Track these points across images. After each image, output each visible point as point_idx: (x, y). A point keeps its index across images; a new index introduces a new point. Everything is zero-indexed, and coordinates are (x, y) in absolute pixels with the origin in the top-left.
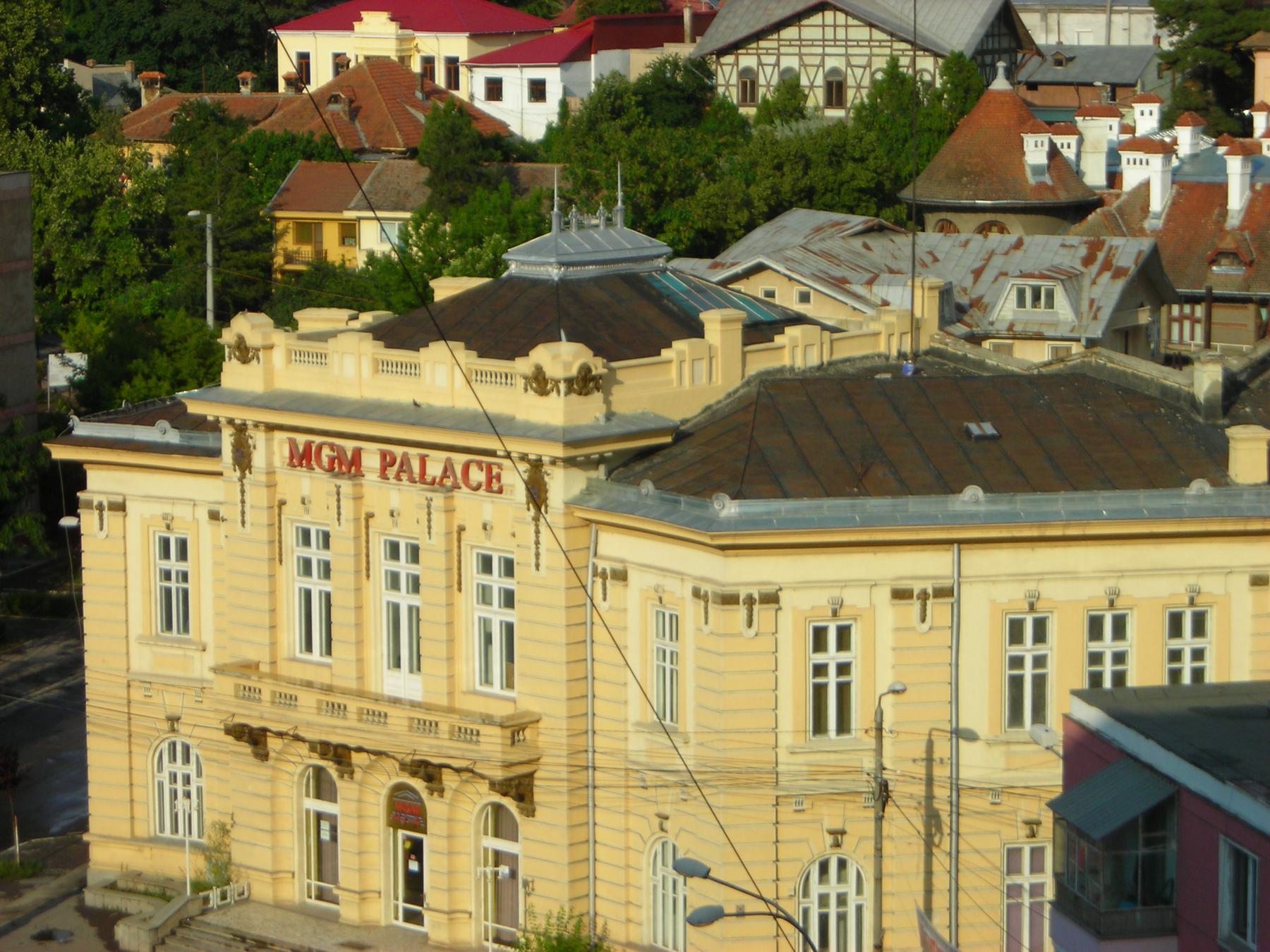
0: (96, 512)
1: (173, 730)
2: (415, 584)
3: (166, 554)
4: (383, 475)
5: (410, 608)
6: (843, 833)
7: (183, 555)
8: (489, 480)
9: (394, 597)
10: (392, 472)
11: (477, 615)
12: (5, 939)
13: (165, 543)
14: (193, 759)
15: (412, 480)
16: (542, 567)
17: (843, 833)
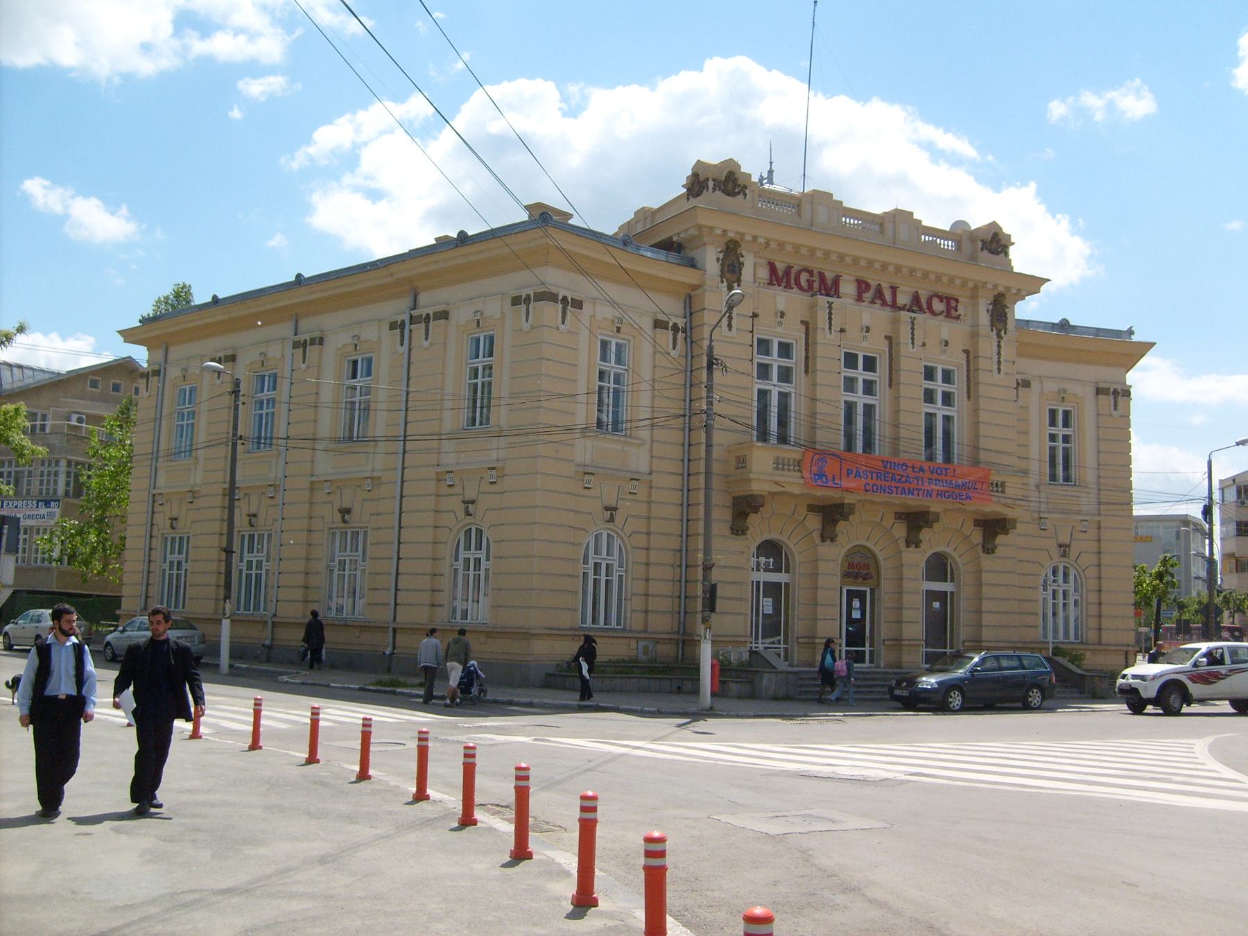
0: (560, 306)
1: (468, 514)
2: (948, 399)
3: (1053, 423)
4: (859, 299)
5: (865, 405)
6: (615, 509)
7: (1066, 424)
8: (949, 308)
9: (929, 409)
10: (868, 296)
11: (756, 387)
12: (4, 831)
13: (1053, 413)
14: (1071, 578)
15: (884, 303)
16: (734, 329)
17: (615, 509)
